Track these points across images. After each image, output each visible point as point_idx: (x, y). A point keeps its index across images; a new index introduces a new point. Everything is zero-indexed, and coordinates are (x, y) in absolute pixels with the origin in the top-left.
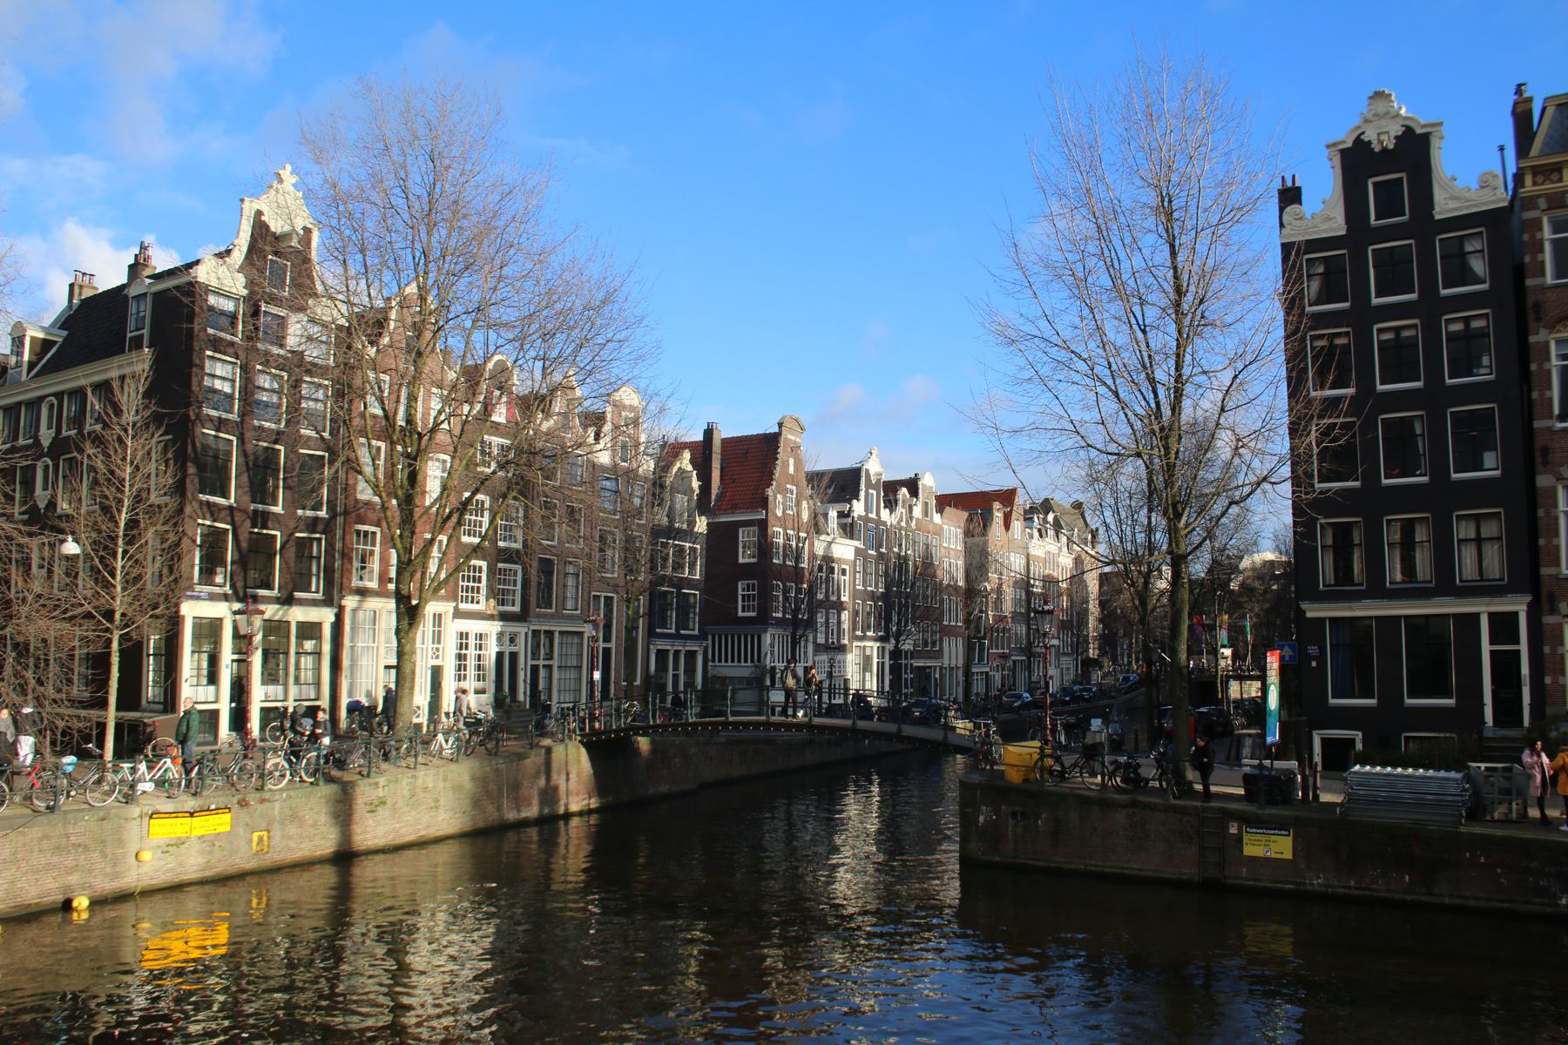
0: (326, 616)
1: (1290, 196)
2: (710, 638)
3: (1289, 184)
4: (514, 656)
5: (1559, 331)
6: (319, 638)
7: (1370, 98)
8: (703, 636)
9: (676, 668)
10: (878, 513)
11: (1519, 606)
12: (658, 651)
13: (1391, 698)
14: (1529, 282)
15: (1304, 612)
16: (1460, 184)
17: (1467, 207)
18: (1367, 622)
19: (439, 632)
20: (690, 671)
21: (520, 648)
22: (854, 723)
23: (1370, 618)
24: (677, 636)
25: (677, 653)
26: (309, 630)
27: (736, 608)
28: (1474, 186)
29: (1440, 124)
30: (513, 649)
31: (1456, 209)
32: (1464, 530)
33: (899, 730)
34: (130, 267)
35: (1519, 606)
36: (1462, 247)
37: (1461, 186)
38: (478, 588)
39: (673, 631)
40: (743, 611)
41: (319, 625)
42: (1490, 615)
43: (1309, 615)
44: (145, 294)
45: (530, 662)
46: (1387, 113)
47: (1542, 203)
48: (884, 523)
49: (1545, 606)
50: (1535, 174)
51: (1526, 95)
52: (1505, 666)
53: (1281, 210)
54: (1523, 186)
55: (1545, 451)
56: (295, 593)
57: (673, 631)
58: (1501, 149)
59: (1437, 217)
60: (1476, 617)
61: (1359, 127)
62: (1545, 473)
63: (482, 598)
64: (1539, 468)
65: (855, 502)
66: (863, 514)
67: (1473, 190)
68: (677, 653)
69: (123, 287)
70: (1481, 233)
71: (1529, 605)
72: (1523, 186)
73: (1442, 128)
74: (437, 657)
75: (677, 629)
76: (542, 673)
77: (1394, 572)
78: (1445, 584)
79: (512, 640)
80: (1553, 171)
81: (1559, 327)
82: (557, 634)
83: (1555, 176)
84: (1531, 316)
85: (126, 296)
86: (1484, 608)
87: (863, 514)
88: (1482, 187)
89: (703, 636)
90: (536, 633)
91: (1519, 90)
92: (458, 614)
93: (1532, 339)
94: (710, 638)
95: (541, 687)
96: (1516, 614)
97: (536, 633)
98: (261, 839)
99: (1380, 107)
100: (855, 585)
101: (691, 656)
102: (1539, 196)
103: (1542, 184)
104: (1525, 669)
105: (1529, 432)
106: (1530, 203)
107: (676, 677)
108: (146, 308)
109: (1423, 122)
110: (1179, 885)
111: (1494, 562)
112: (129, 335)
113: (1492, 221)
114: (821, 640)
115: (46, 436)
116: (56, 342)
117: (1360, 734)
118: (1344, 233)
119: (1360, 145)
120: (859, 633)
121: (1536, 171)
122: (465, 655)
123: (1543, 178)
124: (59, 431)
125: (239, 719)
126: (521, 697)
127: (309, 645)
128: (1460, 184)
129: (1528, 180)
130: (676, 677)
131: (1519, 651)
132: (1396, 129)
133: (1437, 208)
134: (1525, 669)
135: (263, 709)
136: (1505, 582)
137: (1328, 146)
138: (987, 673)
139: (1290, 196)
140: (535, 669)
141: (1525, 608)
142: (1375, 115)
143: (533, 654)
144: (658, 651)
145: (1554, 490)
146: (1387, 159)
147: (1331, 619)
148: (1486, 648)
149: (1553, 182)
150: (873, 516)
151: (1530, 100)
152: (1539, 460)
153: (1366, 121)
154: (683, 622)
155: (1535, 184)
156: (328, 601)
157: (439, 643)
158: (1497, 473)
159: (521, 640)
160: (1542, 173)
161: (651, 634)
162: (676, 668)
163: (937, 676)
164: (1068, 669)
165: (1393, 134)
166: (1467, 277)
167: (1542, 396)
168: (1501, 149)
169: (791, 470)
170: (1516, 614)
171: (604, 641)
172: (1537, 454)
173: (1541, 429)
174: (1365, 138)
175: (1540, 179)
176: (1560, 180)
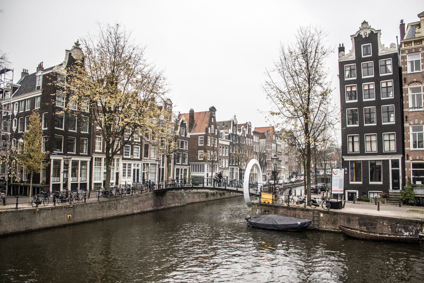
0: (88, 159)
1: (341, 49)
2: (191, 165)
3: (341, 46)
4: (138, 170)
5: (411, 85)
6: (86, 165)
7: (362, 24)
8: (189, 165)
9: (181, 173)
10: (236, 133)
11: (399, 158)
12: (177, 169)
13: (366, 182)
14: (403, 73)
15: (344, 159)
16: (385, 46)
17: (387, 53)
18: (360, 162)
19: (118, 164)
20: (185, 174)
21: (140, 168)
22: (237, 189)
23: (361, 161)
24: (182, 165)
25: (182, 169)
26: (84, 163)
27: (198, 157)
28: (389, 47)
29: (380, 30)
30: (138, 168)
31: (384, 53)
32: (386, 138)
33: (237, 189)
34: (37, 68)
35: (399, 158)
36: (385, 63)
37: (386, 47)
38: (129, 152)
39: (181, 163)
40: (200, 158)
41: (87, 161)
42: (392, 160)
43: (345, 160)
44: (41, 75)
45: (142, 172)
46: (366, 27)
47: (407, 52)
48: (238, 135)
49: (406, 158)
50: (405, 44)
51: (403, 23)
52: (395, 174)
53: (339, 53)
54: (402, 47)
55: (407, 117)
56: (205, 133)
57: (181, 163)
58: (397, 37)
59: (379, 55)
60: (388, 161)
61: (359, 31)
62: (406, 123)
63: (130, 155)
64: (405, 121)
65: (229, 129)
66: (232, 133)
67: (389, 48)
68: (182, 169)
69: (35, 73)
70: (391, 59)
71: (402, 157)
72: (402, 47)
73: (381, 32)
74: (118, 170)
75: (182, 163)
76: (145, 174)
77: (350, 149)
78: (380, 151)
79: (138, 166)
80: (409, 43)
81: (411, 84)
82: (149, 164)
83: (410, 45)
84: (403, 81)
85: (36, 76)
86: (390, 158)
87: (232, 133)
88: (391, 47)
89: (189, 165)
90: (144, 164)
91: (402, 21)
92: (123, 159)
93: (403, 88)
94: (191, 165)
95: (145, 178)
96: (398, 160)
97: (144, 164)
98: (70, 216)
99: (365, 26)
100: (230, 151)
101: (186, 170)
102: (406, 50)
103: (407, 46)
104: (401, 174)
105: (402, 112)
106: (403, 52)
107: (181, 176)
108: (41, 78)
109: (376, 30)
110: (150, 211)
111: (393, 147)
112: (37, 86)
113: (394, 57)
114: (220, 166)
115: (15, 113)
116: (18, 88)
117: (358, 191)
118: (355, 59)
119: (359, 36)
120: (231, 164)
121: (405, 43)
122: (130, 170)
123: (407, 45)
124: (19, 111)
125: (65, 186)
126: (140, 181)
127: (83, 167)
128: (385, 46)
129: (403, 45)
130: (181, 176)
131: (399, 170)
132: (369, 32)
133: (379, 53)
134: (401, 174)
135: (53, 184)
136: (396, 152)
137: (351, 36)
138: (265, 175)
139: (341, 49)
140: (144, 174)
141: (401, 158)
142: (363, 28)
143: (143, 169)
144: (177, 169)
145: (409, 127)
146: (367, 40)
147: (350, 161)
148: (390, 169)
149: (410, 46)
150: (235, 133)
151: (404, 24)
152: (405, 119)
153: (361, 29)
154: (183, 161)
155: (405, 46)
156: (89, 155)
157: (118, 166)
158: (394, 123)
159: (140, 166)
160: (407, 44)
161: (175, 164)
162: (181, 173)
163: (252, 176)
164: (287, 174)
165: (368, 33)
166: (386, 71)
167: (406, 102)
168: (397, 37)
169: (213, 121)
170: (398, 160)
171: (162, 166)
172: (405, 118)
173: (406, 111)
174: (361, 34)
175: (406, 45)
176: (422, 44)
